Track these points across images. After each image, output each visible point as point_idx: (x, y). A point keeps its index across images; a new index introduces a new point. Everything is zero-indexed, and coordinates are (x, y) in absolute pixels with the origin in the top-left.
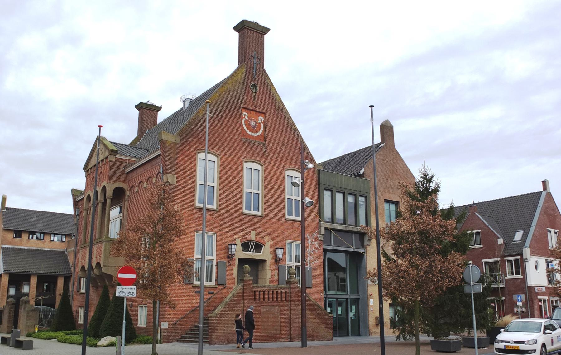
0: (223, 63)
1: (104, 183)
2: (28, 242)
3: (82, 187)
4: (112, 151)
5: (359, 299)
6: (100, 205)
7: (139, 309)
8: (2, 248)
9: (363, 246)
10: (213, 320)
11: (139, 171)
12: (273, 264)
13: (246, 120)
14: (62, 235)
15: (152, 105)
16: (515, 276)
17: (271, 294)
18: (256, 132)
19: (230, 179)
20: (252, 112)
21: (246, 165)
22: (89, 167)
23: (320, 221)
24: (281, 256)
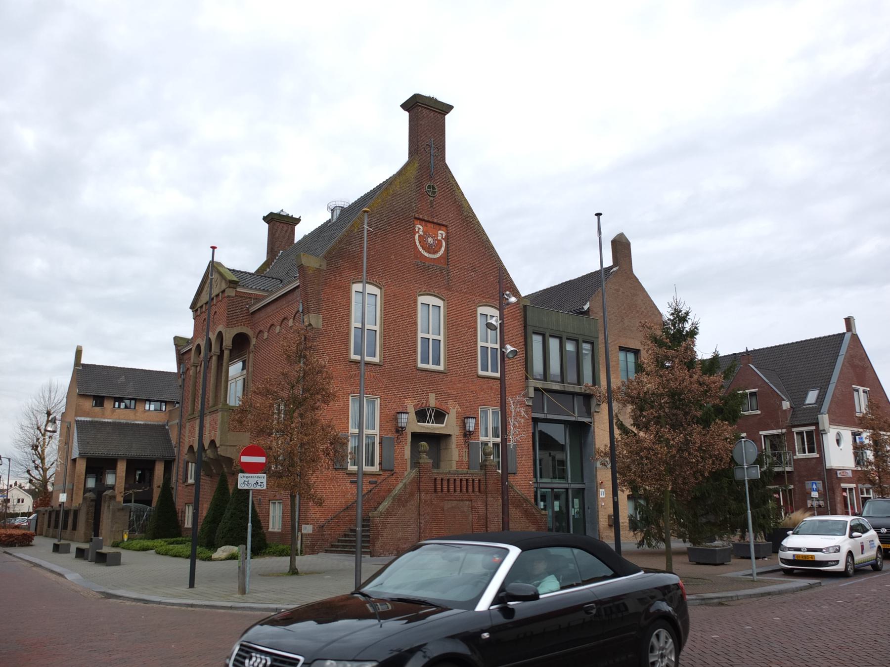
0: (386, 153)
1: (220, 328)
2: (113, 412)
3: (188, 331)
4: (231, 282)
5: (584, 489)
6: (214, 359)
7: (271, 506)
8: (77, 421)
9: (589, 414)
10: (377, 520)
11: (269, 310)
12: (461, 440)
13: (420, 236)
14: (161, 402)
15: (287, 216)
16: (808, 455)
17: (458, 483)
18: (435, 252)
19: (399, 320)
20: (429, 225)
21: (422, 299)
22: (199, 305)
23: (527, 378)
24: (472, 429)
